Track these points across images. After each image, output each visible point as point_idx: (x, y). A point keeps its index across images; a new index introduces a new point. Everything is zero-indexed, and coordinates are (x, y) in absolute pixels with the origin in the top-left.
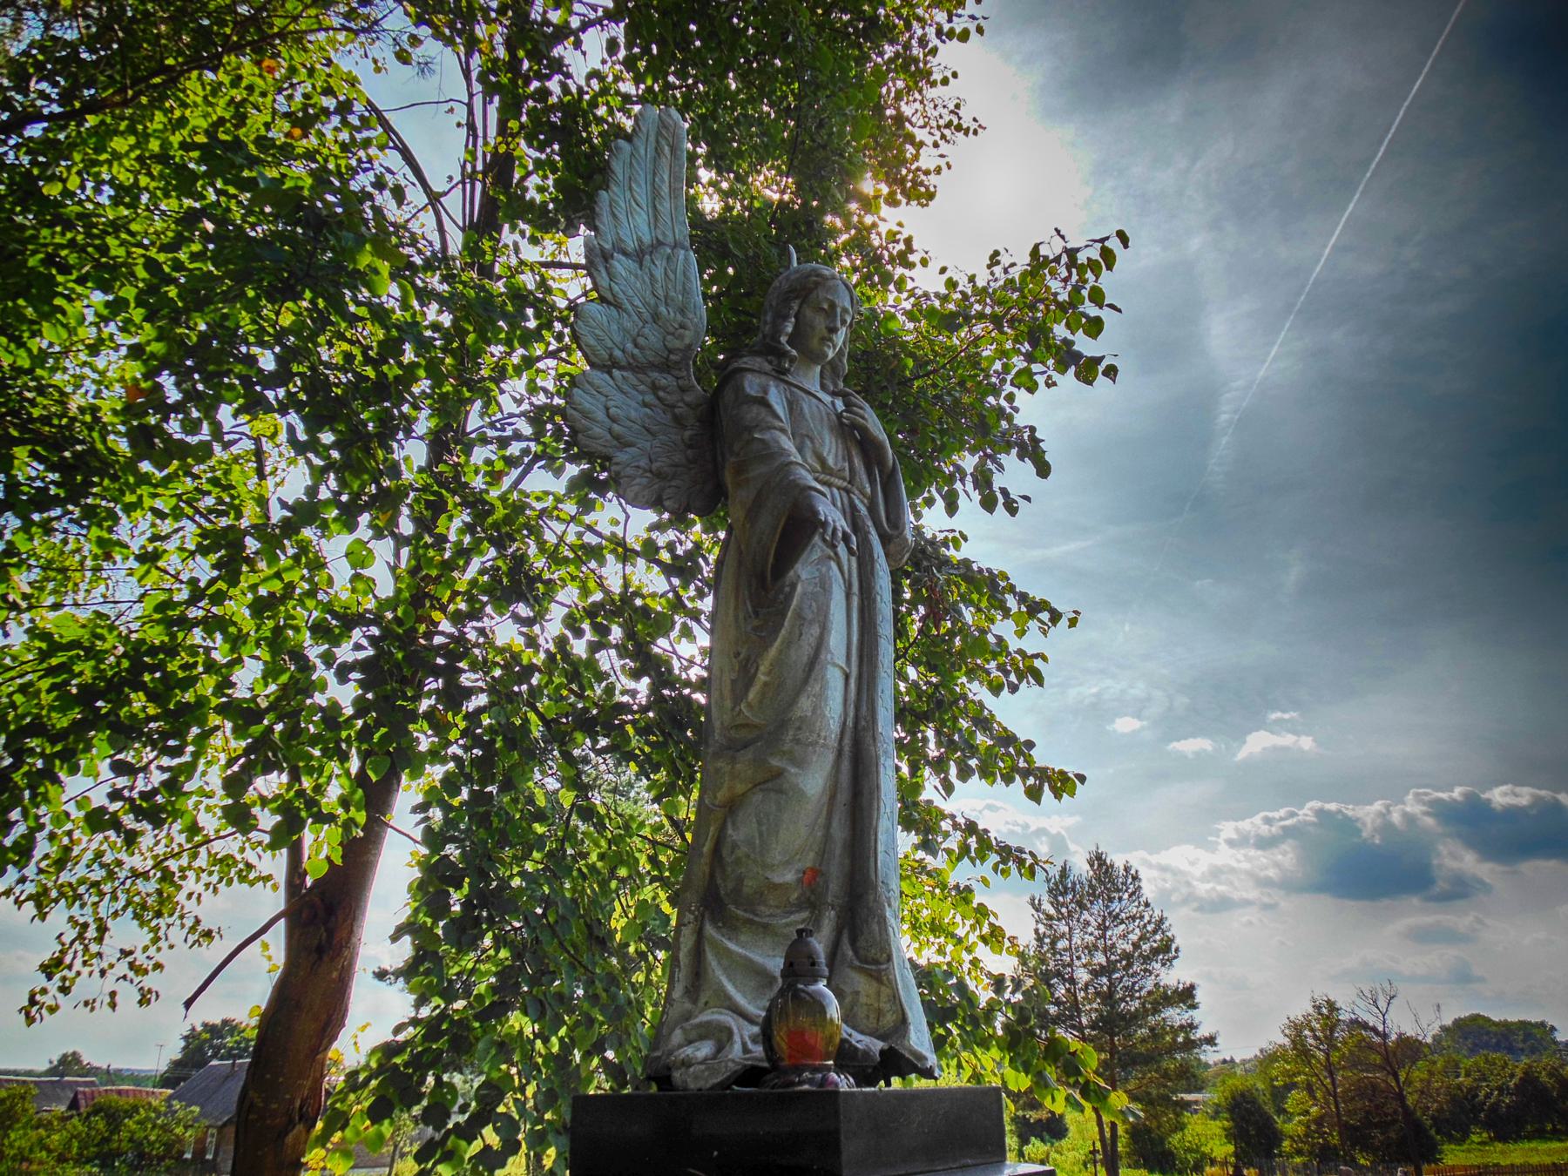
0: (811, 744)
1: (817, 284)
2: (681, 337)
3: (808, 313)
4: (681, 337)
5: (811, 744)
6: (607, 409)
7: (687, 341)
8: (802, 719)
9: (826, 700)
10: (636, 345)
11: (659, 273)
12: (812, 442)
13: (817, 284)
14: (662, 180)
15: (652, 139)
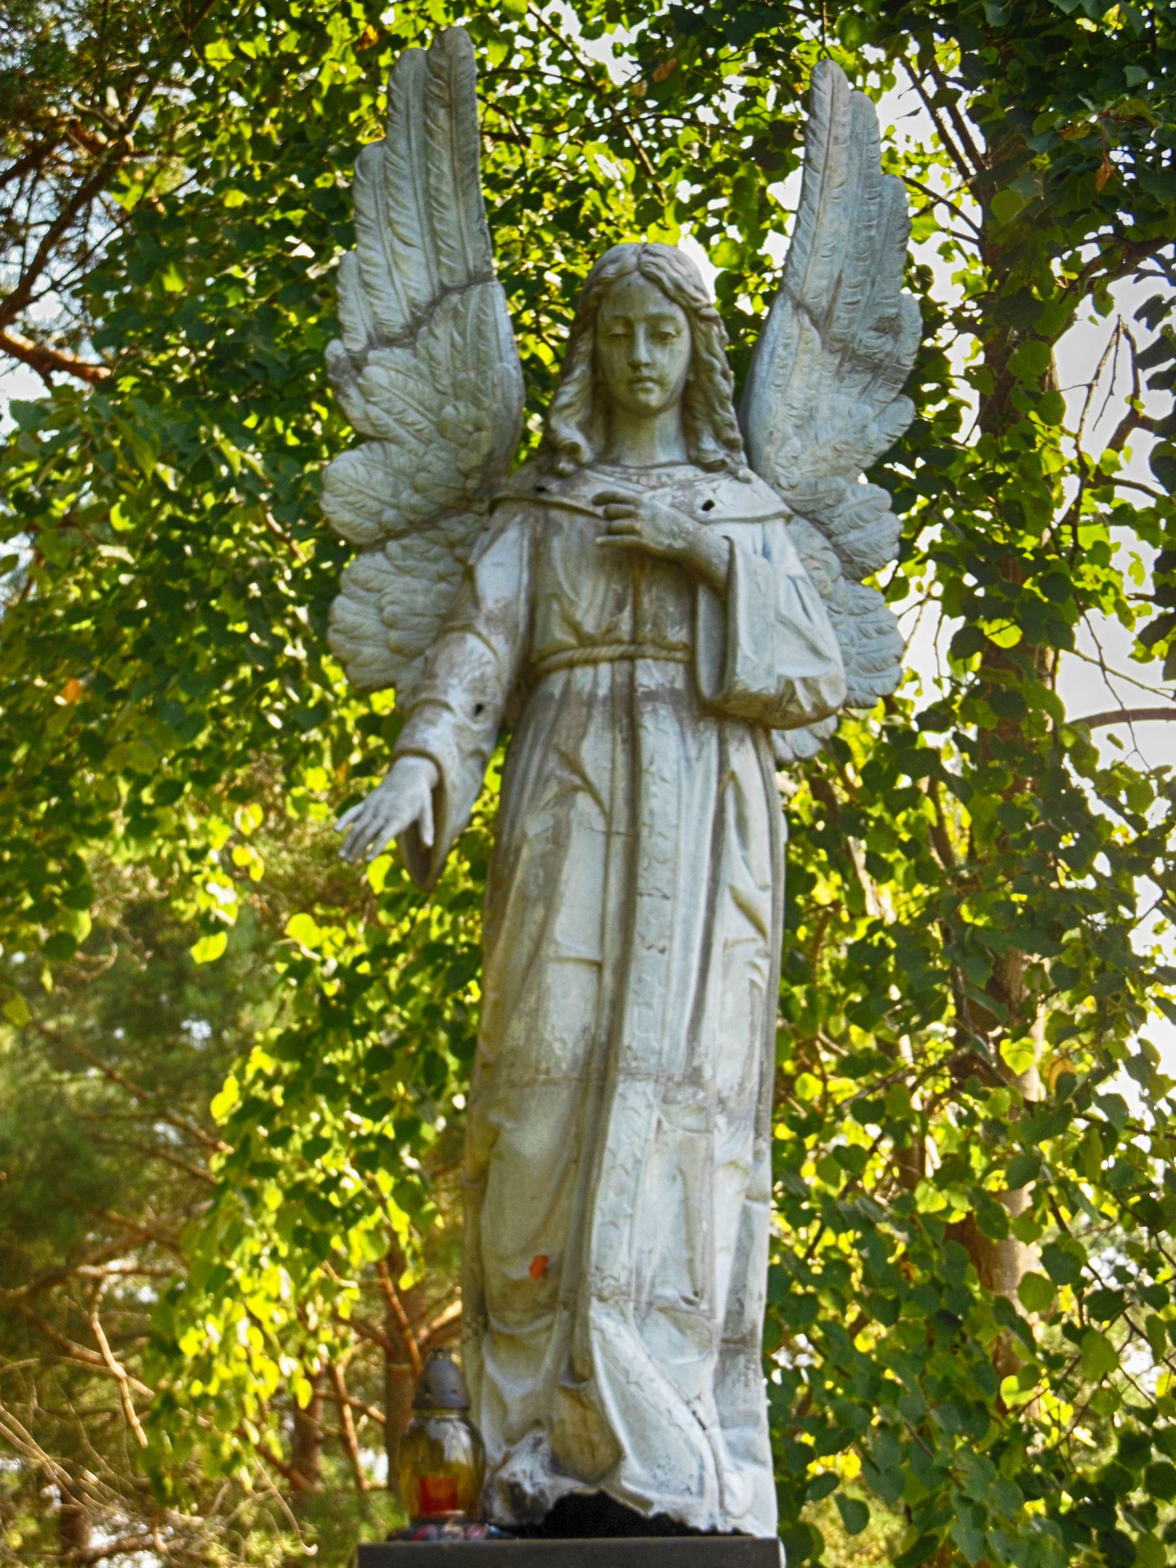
0: (527, 1084)
1: (599, 297)
2: (475, 447)
3: (604, 347)
4: (475, 447)
5: (527, 1084)
6: (381, 610)
7: (485, 449)
8: (514, 1051)
9: (546, 1015)
10: (417, 490)
11: (441, 350)
12: (561, 604)
13: (599, 297)
14: (440, 177)
15: (416, 110)
